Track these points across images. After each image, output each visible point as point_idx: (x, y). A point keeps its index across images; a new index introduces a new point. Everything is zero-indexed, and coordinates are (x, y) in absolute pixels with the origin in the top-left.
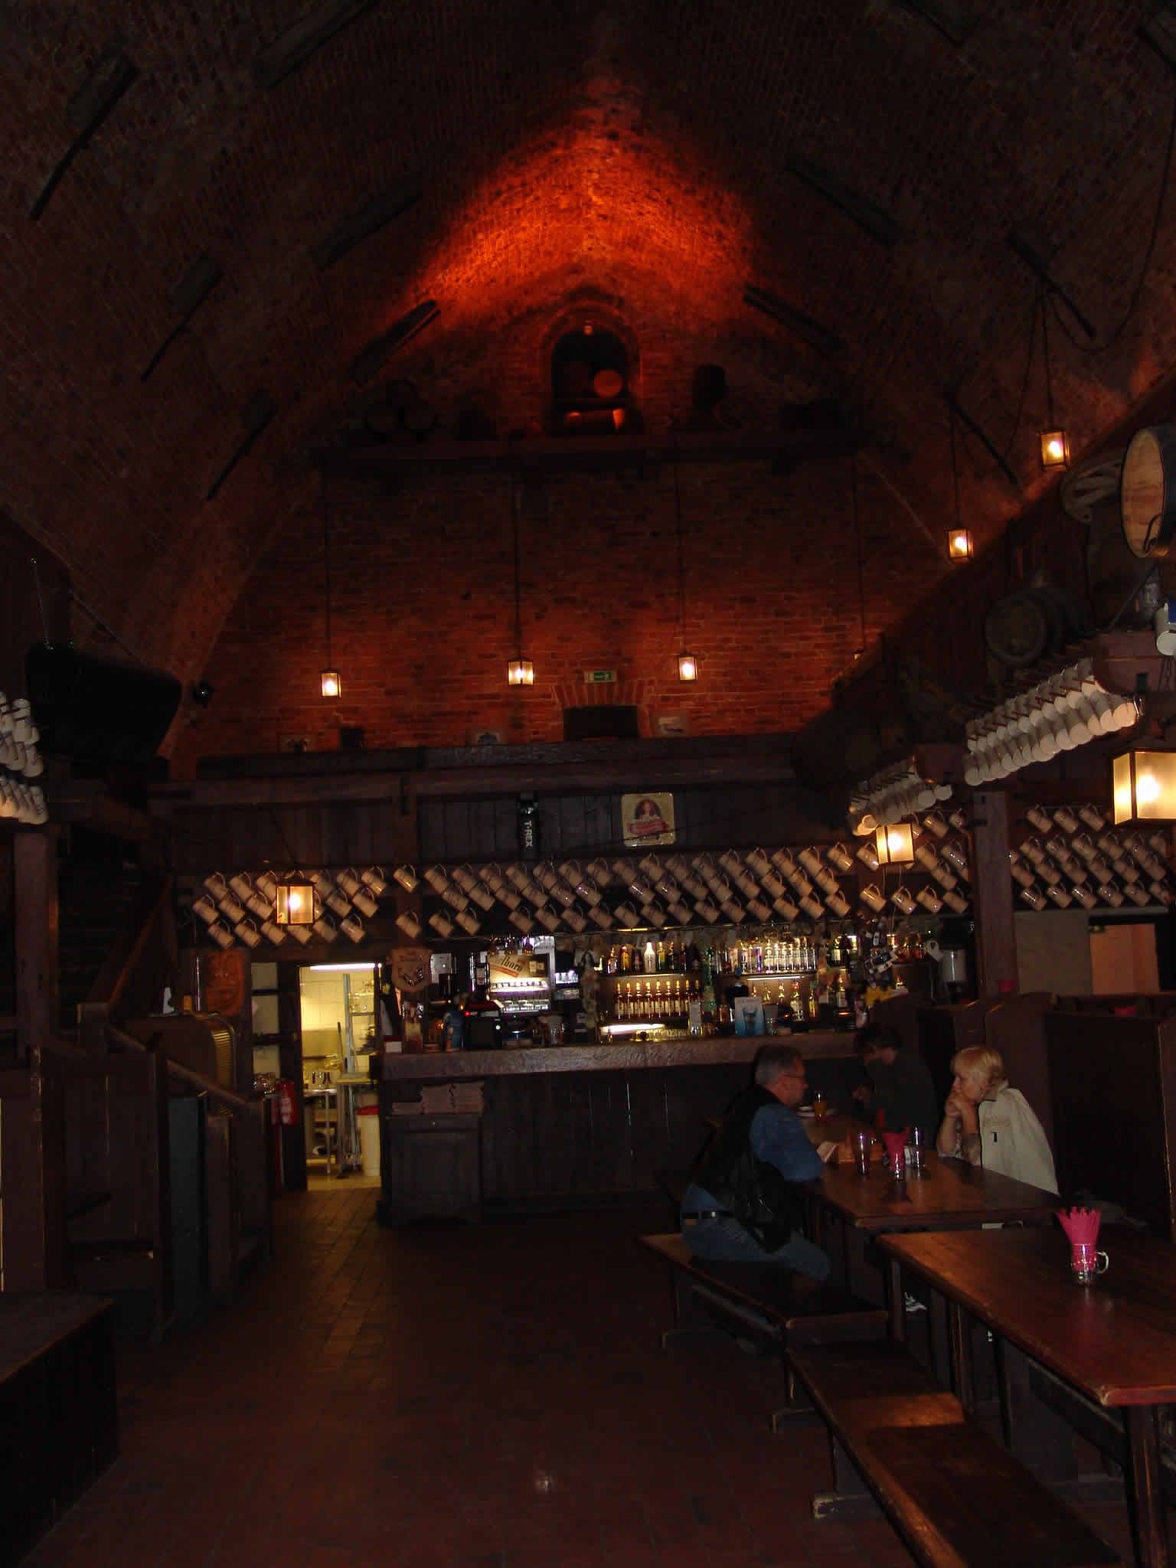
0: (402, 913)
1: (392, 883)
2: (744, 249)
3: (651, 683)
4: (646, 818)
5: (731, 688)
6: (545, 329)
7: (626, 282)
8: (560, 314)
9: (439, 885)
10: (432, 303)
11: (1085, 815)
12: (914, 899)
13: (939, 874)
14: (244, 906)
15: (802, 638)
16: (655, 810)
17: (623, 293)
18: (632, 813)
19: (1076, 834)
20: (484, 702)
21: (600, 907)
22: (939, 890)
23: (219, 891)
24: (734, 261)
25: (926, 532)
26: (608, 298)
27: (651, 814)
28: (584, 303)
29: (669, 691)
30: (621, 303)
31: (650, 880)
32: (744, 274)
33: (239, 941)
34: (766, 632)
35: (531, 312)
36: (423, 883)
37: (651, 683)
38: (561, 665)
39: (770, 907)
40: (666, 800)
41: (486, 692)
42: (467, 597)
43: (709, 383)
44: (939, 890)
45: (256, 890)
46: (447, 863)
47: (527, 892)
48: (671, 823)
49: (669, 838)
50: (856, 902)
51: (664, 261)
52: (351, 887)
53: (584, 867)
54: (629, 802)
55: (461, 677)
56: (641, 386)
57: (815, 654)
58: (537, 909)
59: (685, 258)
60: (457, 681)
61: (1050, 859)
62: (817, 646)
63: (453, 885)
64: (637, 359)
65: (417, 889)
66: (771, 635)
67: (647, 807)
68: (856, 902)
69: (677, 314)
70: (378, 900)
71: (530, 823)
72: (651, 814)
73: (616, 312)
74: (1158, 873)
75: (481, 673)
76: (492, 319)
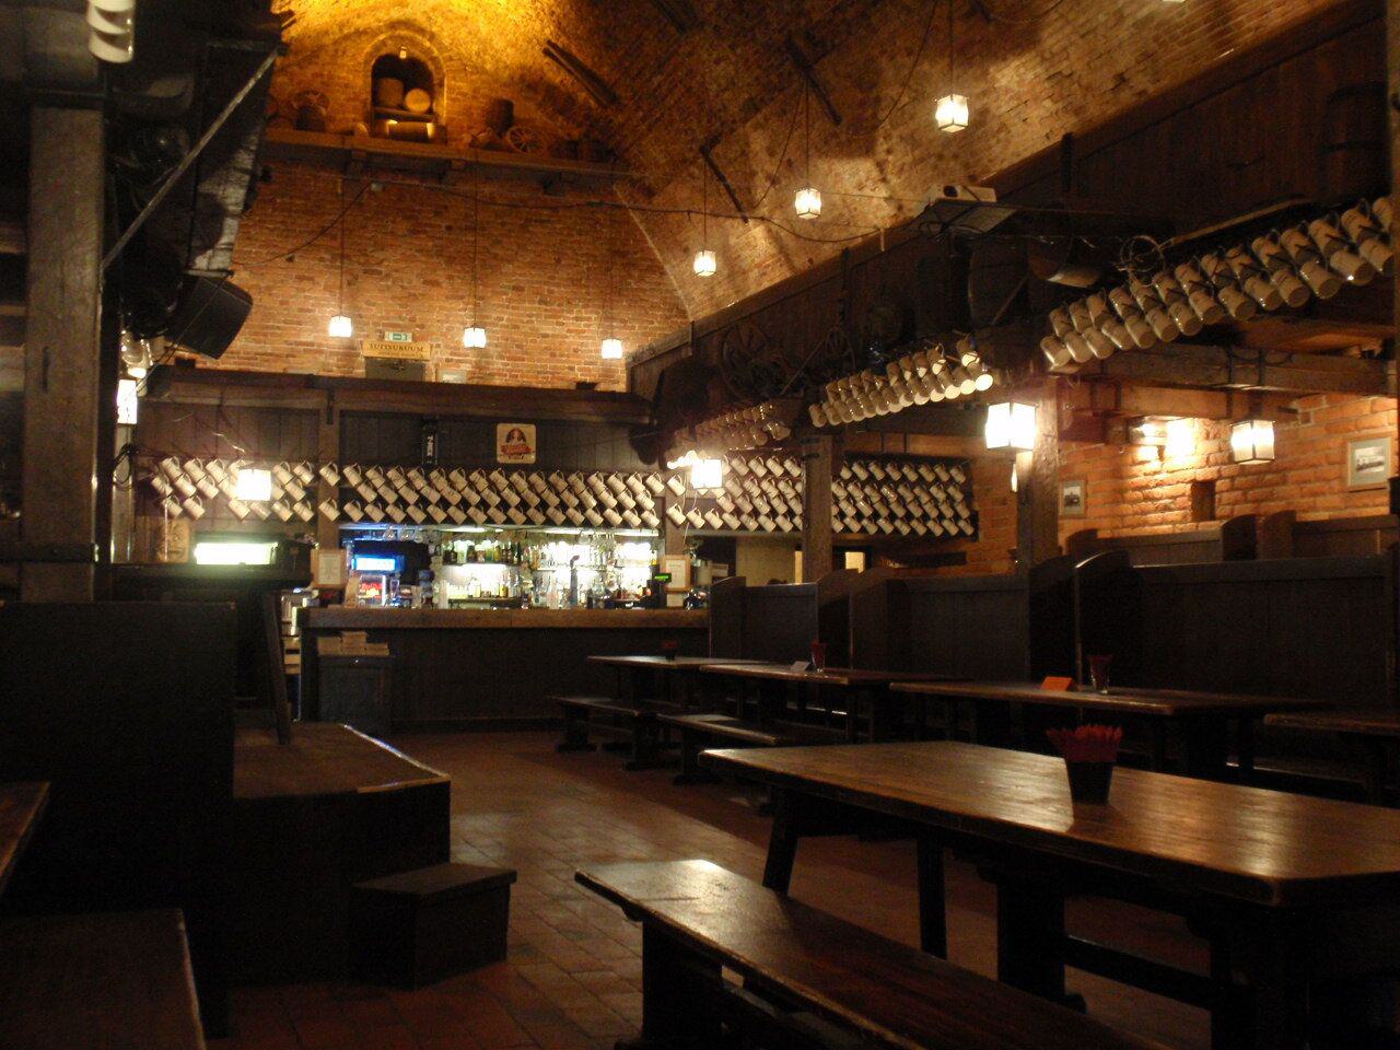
0: (324, 500)
1: (318, 477)
2: (553, 13)
3: (438, 346)
4: (515, 442)
5: (502, 357)
6: (368, 48)
7: (440, 20)
8: (382, 37)
9: (353, 478)
10: (291, 13)
11: (872, 468)
12: (703, 517)
13: (362, 489)
14: (172, 483)
15: (557, 324)
16: (522, 437)
17: (434, 29)
18: (504, 439)
19: (747, 476)
20: (302, 348)
21: (304, 501)
22: (721, 511)
23: (174, 470)
24: (542, 21)
25: (656, 252)
26: (422, 31)
27: (519, 439)
28: (404, 32)
29: (451, 354)
30: (432, 37)
31: (281, 482)
32: (547, 31)
33: (187, 513)
34: (530, 316)
35: (359, 33)
36: (344, 479)
37: (438, 346)
38: (367, 324)
39: (181, 504)
40: (530, 430)
41: (303, 339)
42: (290, 260)
43: (501, 115)
44: (721, 511)
45: (208, 474)
46: (363, 464)
47: (381, 491)
48: (533, 446)
49: (532, 458)
50: (664, 517)
51: (480, 10)
52: (562, 484)
53: (386, 471)
54: (503, 429)
55: (282, 325)
56: (444, 106)
57: (567, 337)
58: (388, 504)
59: (500, 10)
60: (278, 328)
61: (901, 500)
62: (569, 331)
63: (366, 481)
64: (441, 85)
65: (338, 484)
66: (534, 319)
67: (516, 434)
68: (664, 517)
69: (478, 54)
70: (305, 488)
71: (431, 438)
72: (519, 439)
73: (427, 44)
74: (798, 509)
75: (299, 323)
76: (326, 33)
